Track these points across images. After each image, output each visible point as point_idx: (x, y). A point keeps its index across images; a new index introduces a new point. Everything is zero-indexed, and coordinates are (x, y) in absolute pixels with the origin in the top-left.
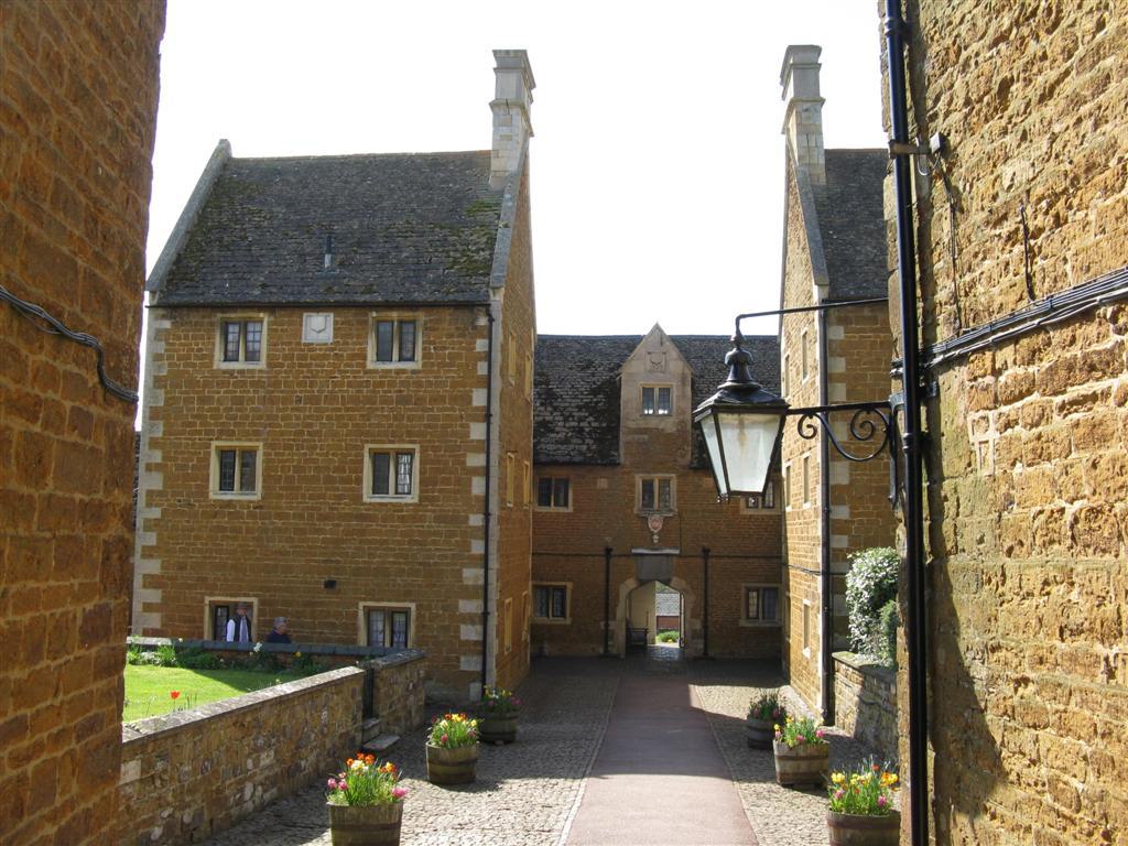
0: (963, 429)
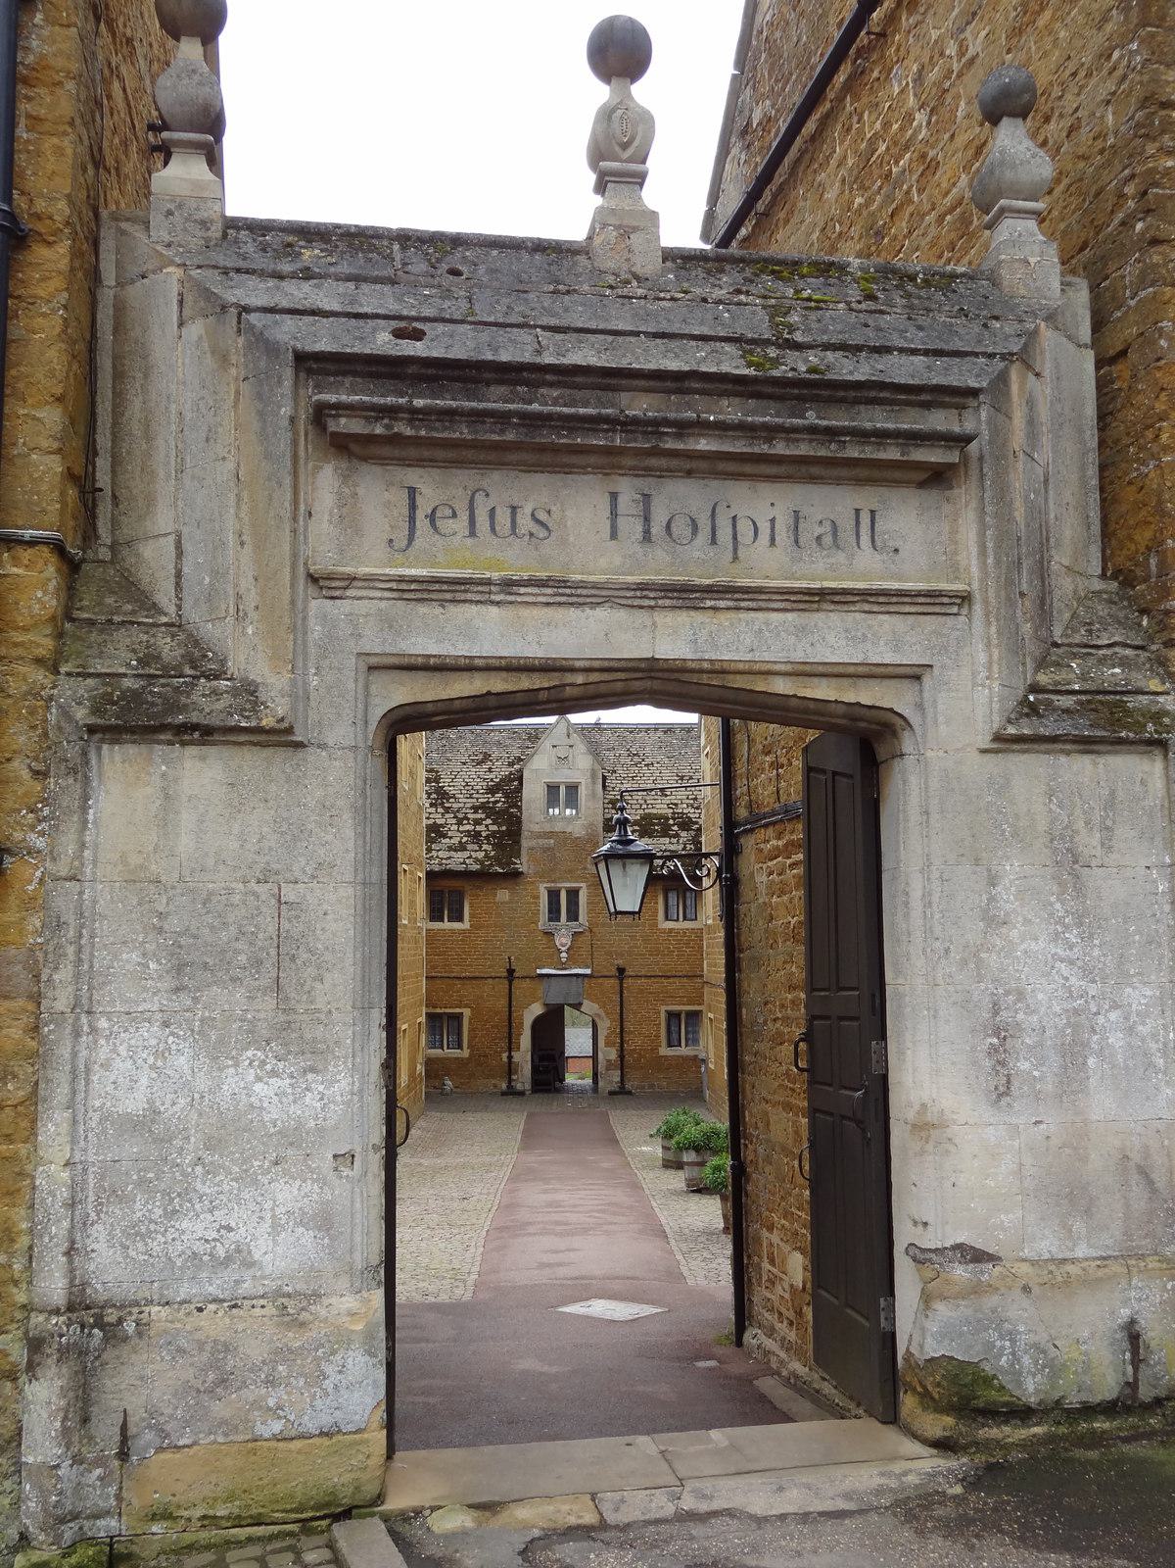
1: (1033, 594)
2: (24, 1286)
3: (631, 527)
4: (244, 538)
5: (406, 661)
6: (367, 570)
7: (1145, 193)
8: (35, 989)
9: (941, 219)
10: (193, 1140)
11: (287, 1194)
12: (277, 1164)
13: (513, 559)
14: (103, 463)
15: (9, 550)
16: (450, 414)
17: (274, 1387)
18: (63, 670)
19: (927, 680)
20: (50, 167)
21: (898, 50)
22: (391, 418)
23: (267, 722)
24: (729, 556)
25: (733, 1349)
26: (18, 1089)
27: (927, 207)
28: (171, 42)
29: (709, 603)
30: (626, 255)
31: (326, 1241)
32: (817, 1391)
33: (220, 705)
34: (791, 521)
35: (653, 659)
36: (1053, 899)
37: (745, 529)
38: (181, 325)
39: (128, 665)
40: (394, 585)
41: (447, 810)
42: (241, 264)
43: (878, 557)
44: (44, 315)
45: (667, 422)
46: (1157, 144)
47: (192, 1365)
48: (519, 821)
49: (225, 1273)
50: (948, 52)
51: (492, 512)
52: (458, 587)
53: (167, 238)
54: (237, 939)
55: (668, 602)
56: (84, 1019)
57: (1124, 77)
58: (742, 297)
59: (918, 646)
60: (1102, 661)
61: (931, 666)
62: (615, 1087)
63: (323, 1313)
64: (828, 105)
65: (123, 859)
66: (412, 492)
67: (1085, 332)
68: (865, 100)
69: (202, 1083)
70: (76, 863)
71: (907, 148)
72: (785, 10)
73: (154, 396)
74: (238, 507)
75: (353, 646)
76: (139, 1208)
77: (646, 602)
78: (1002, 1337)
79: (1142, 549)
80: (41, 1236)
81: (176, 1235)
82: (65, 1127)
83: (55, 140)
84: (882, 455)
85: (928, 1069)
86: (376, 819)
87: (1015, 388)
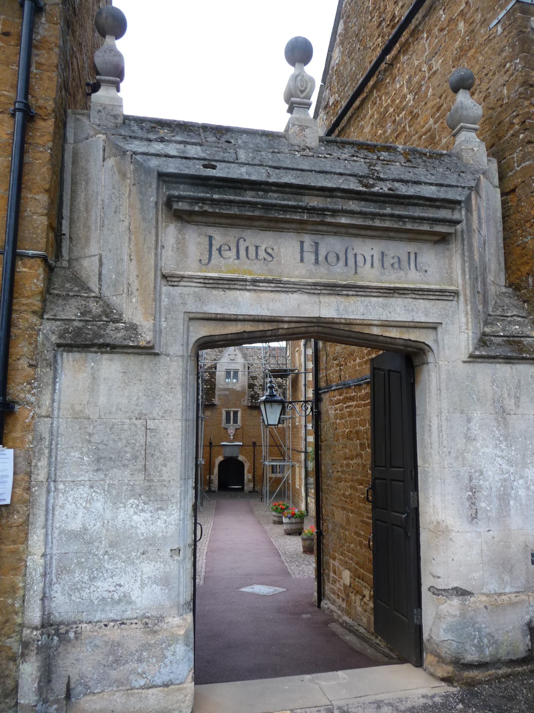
0: (327, 410)
1: (482, 293)
2: (20, 615)
3: (310, 257)
4: (132, 257)
5: (206, 316)
6: (190, 273)
7: (524, 122)
8: (29, 469)
9: (420, 137)
10: (104, 542)
11: (148, 569)
12: (143, 554)
13: (257, 270)
14: (65, 223)
15: (21, 260)
16: (230, 202)
17: (141, 663)
18: (45, 317)
19: (440, 330)
20: (46, 85)
21: (399, 70)
22: (203, 203)
23: (143, 343)
24: (353, 271)
25: (316, 608)
26: (19, 518)
27: (413, 133)
28: (101, 38)
29: (344, 293)
30: (303, 138)
31: (167, 591)
32: (357, 630)
33: (120, 335)
34: (381, 256)
35: (320, 317)
36: (495, 429)
37: (360, 259)
38: (104, 160)
39: (76, 315)
40: (202, 281)
42: (132, 134)
43: (418, 274)
44: (41, 152)
45: (328, 210)
46: (529, 102)
47: (102, 653)
48: (215, 385)
49: (118, 607)
50: (423, 69)
51: (247, 249)
52: (231, 282)
53: (98, 122)
54: (126, 446)
55: (326, 292)
56: (52, 484)
57: (513, 74)
58: (355, 158)
59: (436, 314)
60: (510, 323)
61: (441, 323)
62: (251, 489)
63: (165, 626)
64: (365, 94)
65: (73, 407)
66: (211, 238)
67: (496, 181)
68: (382, 91)
69: (108, 515)
70: (50, 409)
71: (403, 109)
72: (344, 58)
73: (90, 192)
74: (130, 243)
75: (183, 309)
76: (77, 577)
77: (317, 292)
78: (474, 631)
79: (524, 274)
80: (29, 591)
81: (95, 589)
82: (42, 538)
83: (49, 74)
84: (422, 228)
85: (439, 504)
86: (191, 390)
87: (473, 202)
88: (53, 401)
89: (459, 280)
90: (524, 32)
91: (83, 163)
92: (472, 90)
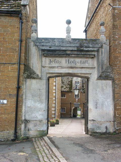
3: (67, 62)
11: (40, 113)
37: (77, 62)
41: (64, 84)
66: (50, 60)
67: (108, 44)
88: (26, 87)
89: (95, 65)
90: (114, 14)
91: (30, 47)
92: (105, 25)
